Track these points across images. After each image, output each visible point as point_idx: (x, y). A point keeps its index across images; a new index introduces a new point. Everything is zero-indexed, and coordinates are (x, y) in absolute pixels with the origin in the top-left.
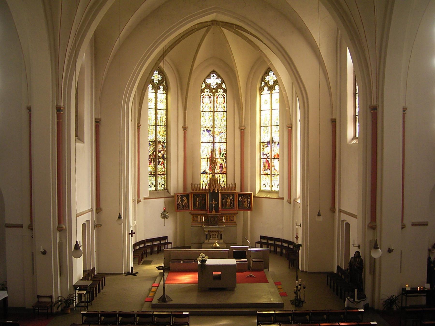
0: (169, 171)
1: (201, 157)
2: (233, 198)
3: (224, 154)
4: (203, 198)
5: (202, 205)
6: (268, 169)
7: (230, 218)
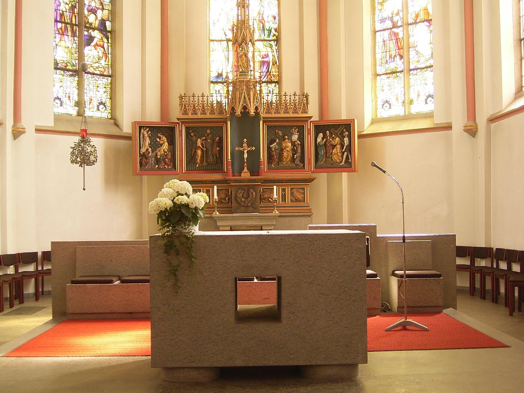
0: (118, 66)
1: (211, 38)
2: (301, 138)
3: (273, 31)
4: (214, 140)
5: (211, 159)
6: (398, 57)
7: (292, 194)
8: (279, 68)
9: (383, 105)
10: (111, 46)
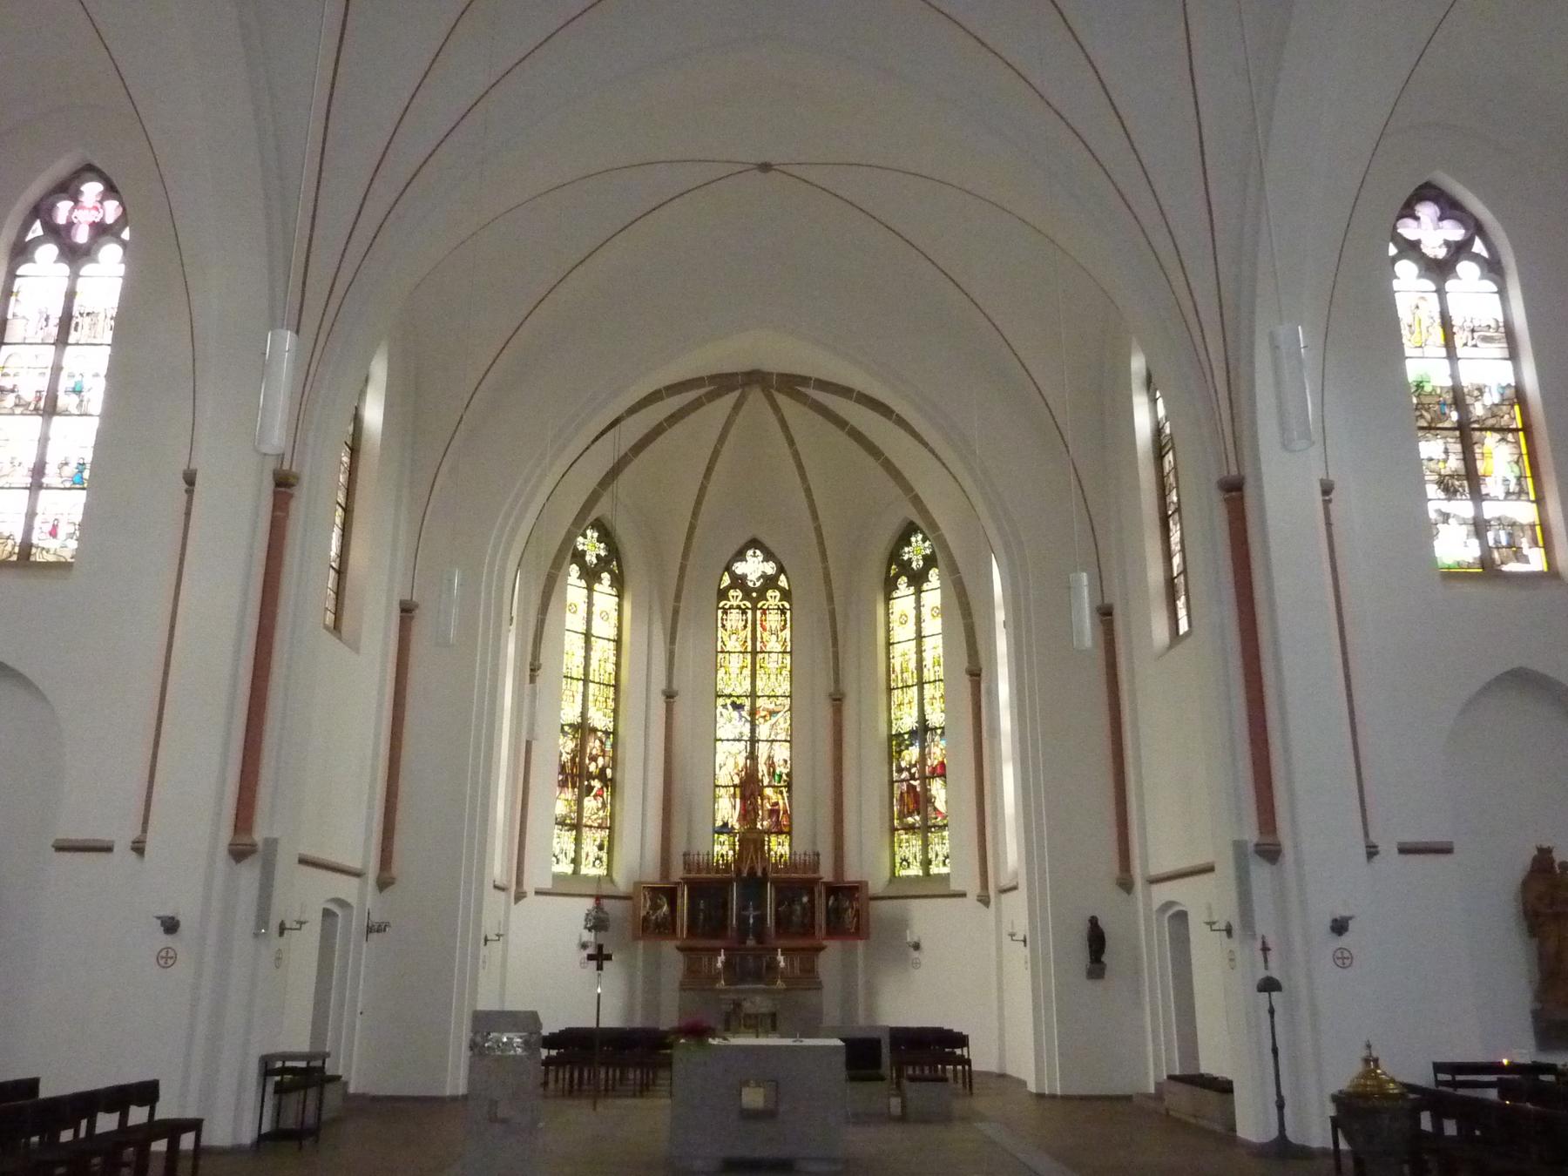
8: (790, 817)
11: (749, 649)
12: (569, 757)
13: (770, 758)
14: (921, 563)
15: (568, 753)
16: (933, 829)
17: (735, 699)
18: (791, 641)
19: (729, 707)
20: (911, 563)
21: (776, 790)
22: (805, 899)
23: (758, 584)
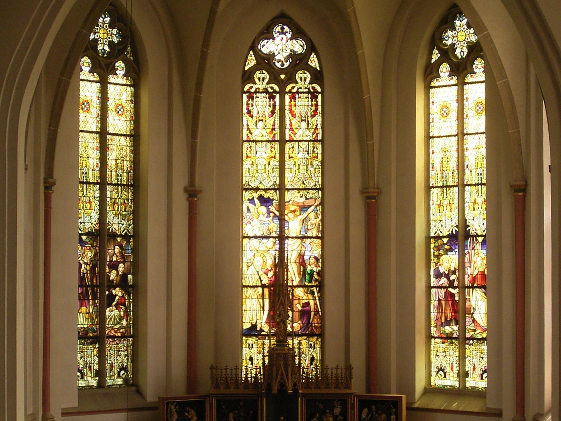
8: (322, 318)
9: (438, 372)
10: (133, 302)
11: (277, 138)
12: (88, 268)
13: (301, 256)
14: (465, 50)
15: (86, 264)
16: (471, 342)
17: (263, 193)
18: (323, 128)
19: (257, 201)
20: (455, 50)
21: (306, 289)
22: (337, 411)
23: (286, 65)
